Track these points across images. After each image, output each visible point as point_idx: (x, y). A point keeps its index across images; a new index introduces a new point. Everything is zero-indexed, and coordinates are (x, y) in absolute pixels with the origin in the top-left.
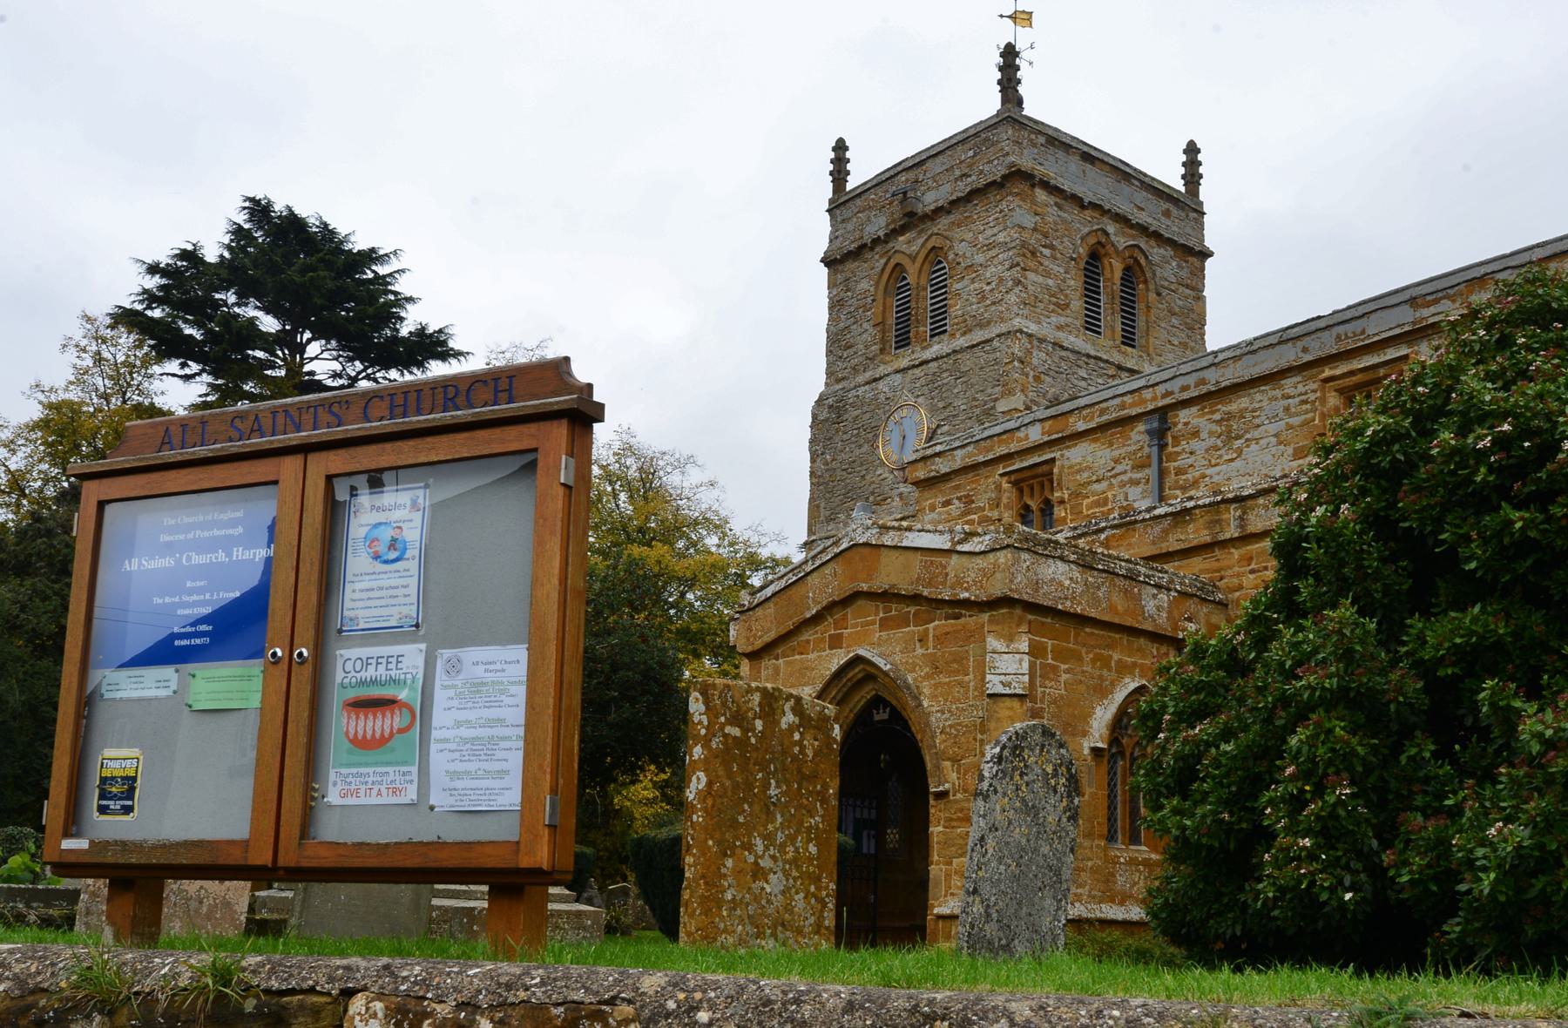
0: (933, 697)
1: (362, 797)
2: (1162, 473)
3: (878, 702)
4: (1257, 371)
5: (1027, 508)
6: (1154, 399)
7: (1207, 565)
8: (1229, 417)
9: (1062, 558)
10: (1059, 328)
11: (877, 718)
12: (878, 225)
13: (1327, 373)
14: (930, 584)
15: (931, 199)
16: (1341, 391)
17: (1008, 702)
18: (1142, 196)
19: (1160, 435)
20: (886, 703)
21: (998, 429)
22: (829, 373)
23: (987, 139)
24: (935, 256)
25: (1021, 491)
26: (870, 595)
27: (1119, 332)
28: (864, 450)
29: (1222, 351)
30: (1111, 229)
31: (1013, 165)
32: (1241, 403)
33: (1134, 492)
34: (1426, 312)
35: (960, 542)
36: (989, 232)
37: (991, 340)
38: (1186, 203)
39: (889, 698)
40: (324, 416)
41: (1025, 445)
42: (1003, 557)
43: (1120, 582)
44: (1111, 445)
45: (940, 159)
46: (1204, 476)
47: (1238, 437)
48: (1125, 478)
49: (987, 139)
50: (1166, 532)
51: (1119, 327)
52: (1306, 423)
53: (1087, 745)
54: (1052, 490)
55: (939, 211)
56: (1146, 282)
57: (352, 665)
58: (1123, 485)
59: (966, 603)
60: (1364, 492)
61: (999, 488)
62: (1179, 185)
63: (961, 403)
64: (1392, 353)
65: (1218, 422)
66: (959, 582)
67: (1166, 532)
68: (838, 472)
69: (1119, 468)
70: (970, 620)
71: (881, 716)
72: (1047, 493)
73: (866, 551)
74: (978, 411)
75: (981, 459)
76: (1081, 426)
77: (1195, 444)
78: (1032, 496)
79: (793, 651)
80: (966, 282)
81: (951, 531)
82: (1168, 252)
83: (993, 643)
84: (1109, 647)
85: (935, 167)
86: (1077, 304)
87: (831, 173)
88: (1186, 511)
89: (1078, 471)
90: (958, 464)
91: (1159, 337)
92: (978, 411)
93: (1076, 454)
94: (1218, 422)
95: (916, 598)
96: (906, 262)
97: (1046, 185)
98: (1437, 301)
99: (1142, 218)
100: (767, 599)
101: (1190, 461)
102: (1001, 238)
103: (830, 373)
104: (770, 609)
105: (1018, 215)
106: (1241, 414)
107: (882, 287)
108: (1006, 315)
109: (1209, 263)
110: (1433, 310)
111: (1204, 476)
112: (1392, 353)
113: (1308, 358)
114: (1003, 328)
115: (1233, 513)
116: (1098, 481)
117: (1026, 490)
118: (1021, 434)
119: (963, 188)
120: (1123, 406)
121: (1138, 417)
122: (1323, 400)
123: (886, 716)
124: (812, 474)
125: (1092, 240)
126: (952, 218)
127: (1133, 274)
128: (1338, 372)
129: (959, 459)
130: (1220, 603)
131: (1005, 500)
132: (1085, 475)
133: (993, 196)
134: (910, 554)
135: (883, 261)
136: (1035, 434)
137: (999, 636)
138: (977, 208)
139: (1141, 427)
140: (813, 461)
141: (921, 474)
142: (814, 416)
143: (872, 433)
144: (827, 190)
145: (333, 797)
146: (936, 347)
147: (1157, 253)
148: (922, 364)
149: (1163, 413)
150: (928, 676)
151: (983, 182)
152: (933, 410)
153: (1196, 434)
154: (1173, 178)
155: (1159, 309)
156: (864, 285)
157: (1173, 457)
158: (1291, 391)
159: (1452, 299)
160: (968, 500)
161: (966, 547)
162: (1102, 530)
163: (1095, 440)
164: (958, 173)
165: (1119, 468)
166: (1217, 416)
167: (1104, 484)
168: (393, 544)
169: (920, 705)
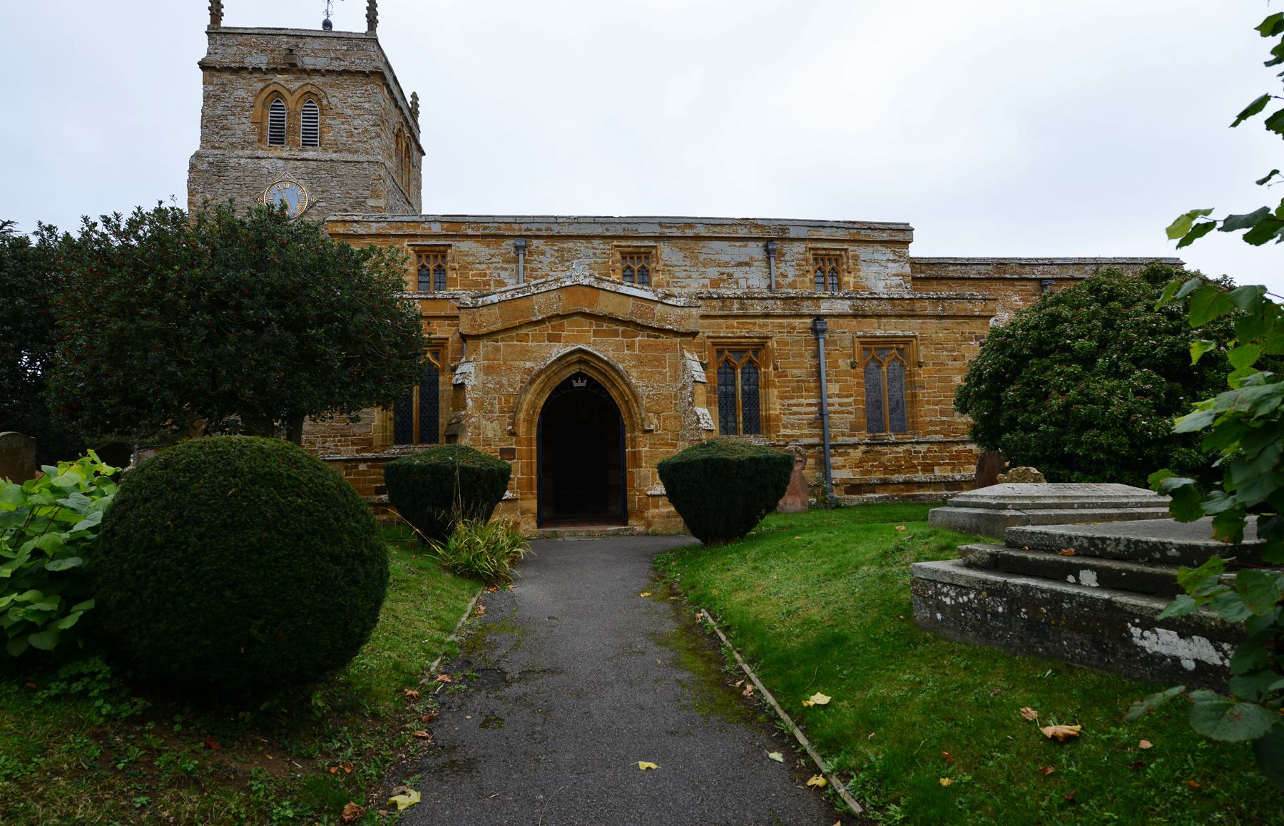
4: (581, 232)
8: (562, 250)
13: (615, 243)
14: (641, 317)
15: (309, 62)
25: (419, 257)
31: (377, 68)
32: (569, 245)
33: (504, 275)
41: (428, 232)
45: (318, 41)
55: (315, 72)
58: (496, 268)
63: (337, 193)
64: (647, 243)
70: (665, 340)
73: (587, 289)
75: (393, 232)
76: (470, 232)
77: (542, 258)
79: (512, 339)
80: (337, 121)
90: (373, 231)
93: (465, 246)
100: (493, 304)
102: (367, 105)
104: (496, 310)
112: (647, 243)
118: (426, 225)
119: (335, 65)
123: (584, 384)
129: (374, 228)
132: (471, 258)
133: (359, 78)
135: (261, 85)
138: (347, 82)
139: (511, 242)
142: (192, 167)
144: (207, 20)
150: (634, 366)
152: (313, 190)
153: (543, 253)
161: (670, 302)
164: (333, 55)
165: (494, 260)
167: (484, 266)
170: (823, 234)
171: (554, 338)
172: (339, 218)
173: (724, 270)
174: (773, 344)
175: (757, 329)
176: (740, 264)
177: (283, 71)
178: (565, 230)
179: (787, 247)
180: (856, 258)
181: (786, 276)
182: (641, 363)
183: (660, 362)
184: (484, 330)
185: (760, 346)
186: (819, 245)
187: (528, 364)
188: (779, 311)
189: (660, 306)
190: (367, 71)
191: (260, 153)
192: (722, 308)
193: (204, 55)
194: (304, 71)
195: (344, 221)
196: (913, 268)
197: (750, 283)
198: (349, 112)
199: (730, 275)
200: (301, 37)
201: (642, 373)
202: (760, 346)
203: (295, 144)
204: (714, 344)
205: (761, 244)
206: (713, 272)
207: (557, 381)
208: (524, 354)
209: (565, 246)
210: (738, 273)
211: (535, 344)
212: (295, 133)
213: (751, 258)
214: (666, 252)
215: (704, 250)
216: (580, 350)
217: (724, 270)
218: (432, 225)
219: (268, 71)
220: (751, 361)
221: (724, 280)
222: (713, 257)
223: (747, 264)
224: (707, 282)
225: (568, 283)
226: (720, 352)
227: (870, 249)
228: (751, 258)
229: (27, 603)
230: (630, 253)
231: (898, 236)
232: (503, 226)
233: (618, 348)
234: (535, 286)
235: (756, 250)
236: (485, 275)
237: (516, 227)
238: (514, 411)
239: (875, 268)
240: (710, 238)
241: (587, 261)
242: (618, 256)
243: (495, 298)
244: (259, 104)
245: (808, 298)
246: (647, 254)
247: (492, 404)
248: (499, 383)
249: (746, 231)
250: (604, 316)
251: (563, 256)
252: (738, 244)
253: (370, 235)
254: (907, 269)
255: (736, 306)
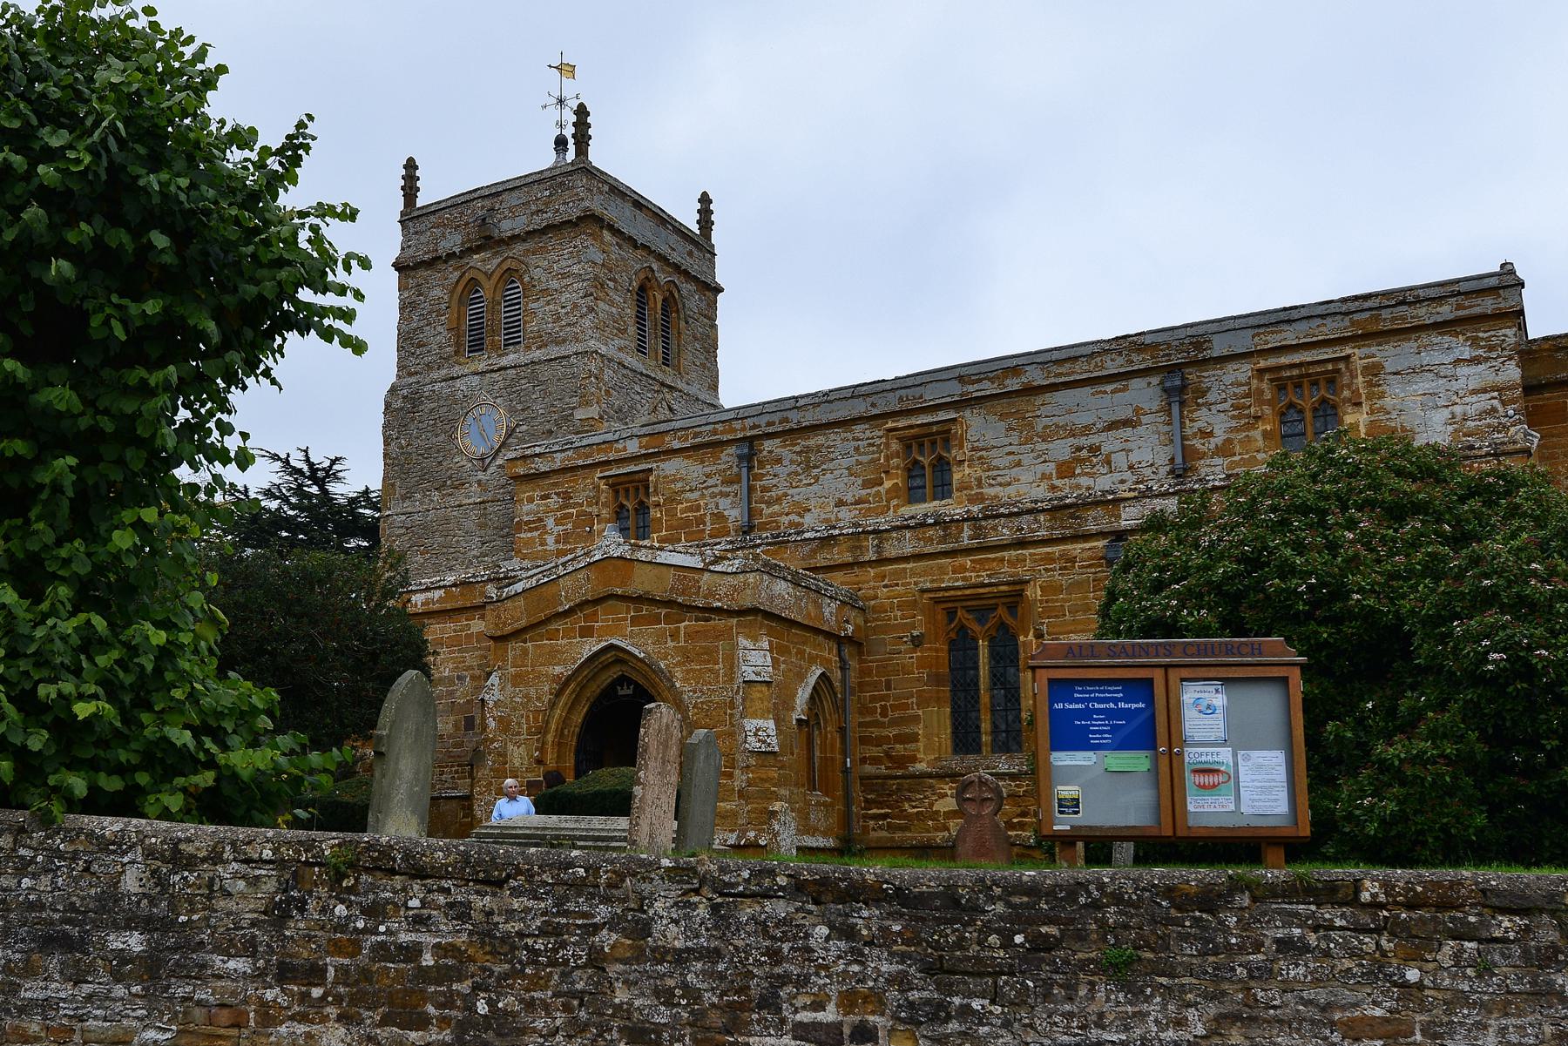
0: (685, 680)
1: (1206, 809)
2: (751, 489)
3: (623, 680)
4: (832, 417)
5: (622, 506)
6: (743, 429)
7: (848, 579)
8: (808, 450)
9: (784, 579)
10: (620, 349)
11: (621, 693)
12: (453, 242)
13: (890, 425)
14: (683, 594)
15: (507, 227)
16: (900, 439)
17: (759, 687)
18: (674, 239)
19: (748, 459)
20: (630, 681)
21: (596, 440)
22: (401, 367)
23: (563, 183)
24: (509, 275)
25: (617, 492)
26: (624, 598)
27: (660, 355)
28: (441, 438)
29: (802, 397)
30: (655, 267)
31: (587, 209)
33: (724, 503)
34: (971, 388)
35: (712, 563)
36: (564, 263)
37: (569, 356)
38: (701, 242)
39: (634, 676)
40: (1162, 651)
41: (623, 455)
42: (751, 578)
43: (812, 595)
44: (703, 462)
45: (516, 194)
46: (786, 495)
47: (816, 467)
48: (716, 490)
49: (563, 183)
50: (814, 552)
51: (660, 350)
52: (872, 461)
53: (795, 716)
54: (647, 494)
56: (677, 311)
57: (1192, 756)
58: (713, 496)
59: (719, 610)
60: (1217, 605)
61: (596, 488)
62: (695, 228)
64: (943, 416)
65: (799, 453)
66: (711, 594)
67: (814, 552)
68: (414, 456)
69: (710, 482)
70: (718, 623)
71: (625, 691)
72: (642, 496)
73: (621, 562)
74: (556, 416)
75: (580, 462)
76: (676, 445)
77: (778, 469)
78: (627, 498)
79: (541, 637)
80: (541, 302)
81: (702, 554)
82: (691, 287)
83: (743, 642)
84: (804, 643)
85: (513, 199)
86: (632, 330)
87: (403, 188)
88: (832, 537)
89: (673, 481)
91: (687, 359)
92: (556, 416)
93: (671, 467)
94: (799, 453)
95: (669, 603)
96: (481, 278)
97: (616, 232)
98: (980, 381)
99: (675, 258)
100: (517, 594)
101: (775, 481)
102: (575, 269)
103: (401, 367)
104: (521, 602)
105: (592, 251)
106: (819, 448)
107: (456, 296)
108: (581, 336)
109: (720, 296)
110: (976, 386)
111: (786, 495)
112: (943, 416)
113: (875, 411)
114: (580, 348)
115: (871, 542)
116: (691, 490)
117: (622, 493)
119: (539, 222)
120: (715, 432)
121: (729, 442)
122: (887, 445)
123: (630, 692)
124: (386, 455)
125: (642, 276)
126: (527, 246)
127: (670, 304)
128: (900, 425)
129: (559, 461)
130: (862, 609)
131: (603, 499)
132: (679, 485)
134: (664, 569)
135: (457, 274)
136: (633, 447)
137: (747, 637)
138: (551, 241)
139: (732, 450)
140: (386, 443)
141: (521, 471)
142: (388, 405)
143: (449, 426)
145: (1191, 808)
146: (512, 356)
147: (687, 287)
148: (500, 369)
149: (750, 440)
151: (558, 219)
152: (511, 411)
153: (779, 461)
154: (691, 221)
155: (686, 335)
156: (437, 292)
157: (760, 477)
158: (861, 436)
159: (992, 380)
160: (566, 496)
161: (718, 568)
162: (759, 546)
163: (688, 457)
164: (534, 208)
165: (710, 482)
166: (797, 448)
167: (696, 495)
168: (1209, 707)
169: (673, 685)
170: (1289, 336)
171: (586, 632)
172: (519, 454)
173: (1083, 441)
174: (1033, 592)
175: (1005, 568)
176: (1113, 426)
177: (478, 249)
178: (809, 418)
179: (1209, 376)
180: (1374, 370)
181: (1211, 434)
182: (687, 657)
183: (710, 655)
184: (508, 629)
185: (1014, 597)
186: (1284, 360)
187: (558, 669)
188: (1042, 533)
189: (707, 575)
190: (574, 218)
191: (457, 370)
192: (943, 540)
193: (397, 252)
194: (502, 242)
195: (524, 457)
196: (1522, 365)
197: (1134, 458)
198: (555, 284)
199: (1094, 450)
200: (498, 194)
201: (688, 672)
202: (1014, 597)
203: (495, 347)
204: (937, 601)
205: (1155, 380)
206: (1062, 449)
207: (594, 689)
208: (553, 656)
209: (811, 442)
210: (1110, 442)
211: (565, 641)
212: (494, 332)
213: (1137, 411)
214: (977, 427)
215: (1043, 411)
216: (612, 647)
217: (1083, 441)
218: (628, 442)
219: (463, 254)
220: (1002, 626)
221: (1081, 461)
222: (1061, 421)
223: (1127, 423)
224: (1051, 468)
225: (597, 558)
226: (951, 614)
227: (1409, 346)
228: (1137, 411)
229: (662, 976)
230: (914, 437)
231: (1487, 304)
232: (720, 427)
233: (660, 638)
234: (564, 564)
235: (1144, 394)
236: (698, 508)
237: (737, 425)
238: (542, 730)
239: (1424, 384)
240: (1054, 387)
241: (846, 462)
242: (895, 446)
243: (519, 587)
244: (454, 304)
245: (1096, 503)
246: (943, 436)
247: (519, 724)
248: (526, 696)
249: (1120, 360)
250: (640, 597)
251: (808, 460)
252: (1109, 388)
253: (554, 472)
254: (1512, 372)
255: (967, 532)
